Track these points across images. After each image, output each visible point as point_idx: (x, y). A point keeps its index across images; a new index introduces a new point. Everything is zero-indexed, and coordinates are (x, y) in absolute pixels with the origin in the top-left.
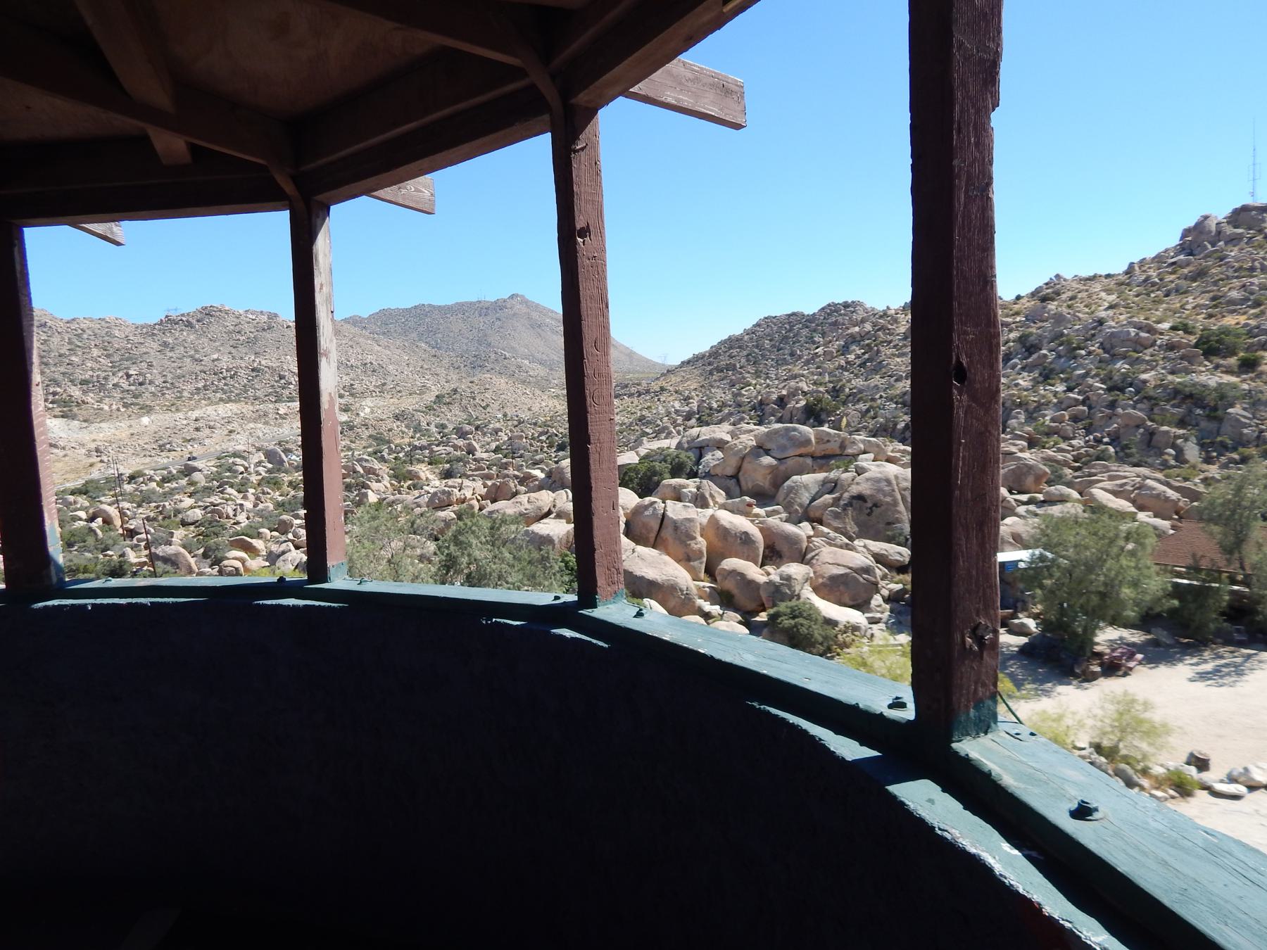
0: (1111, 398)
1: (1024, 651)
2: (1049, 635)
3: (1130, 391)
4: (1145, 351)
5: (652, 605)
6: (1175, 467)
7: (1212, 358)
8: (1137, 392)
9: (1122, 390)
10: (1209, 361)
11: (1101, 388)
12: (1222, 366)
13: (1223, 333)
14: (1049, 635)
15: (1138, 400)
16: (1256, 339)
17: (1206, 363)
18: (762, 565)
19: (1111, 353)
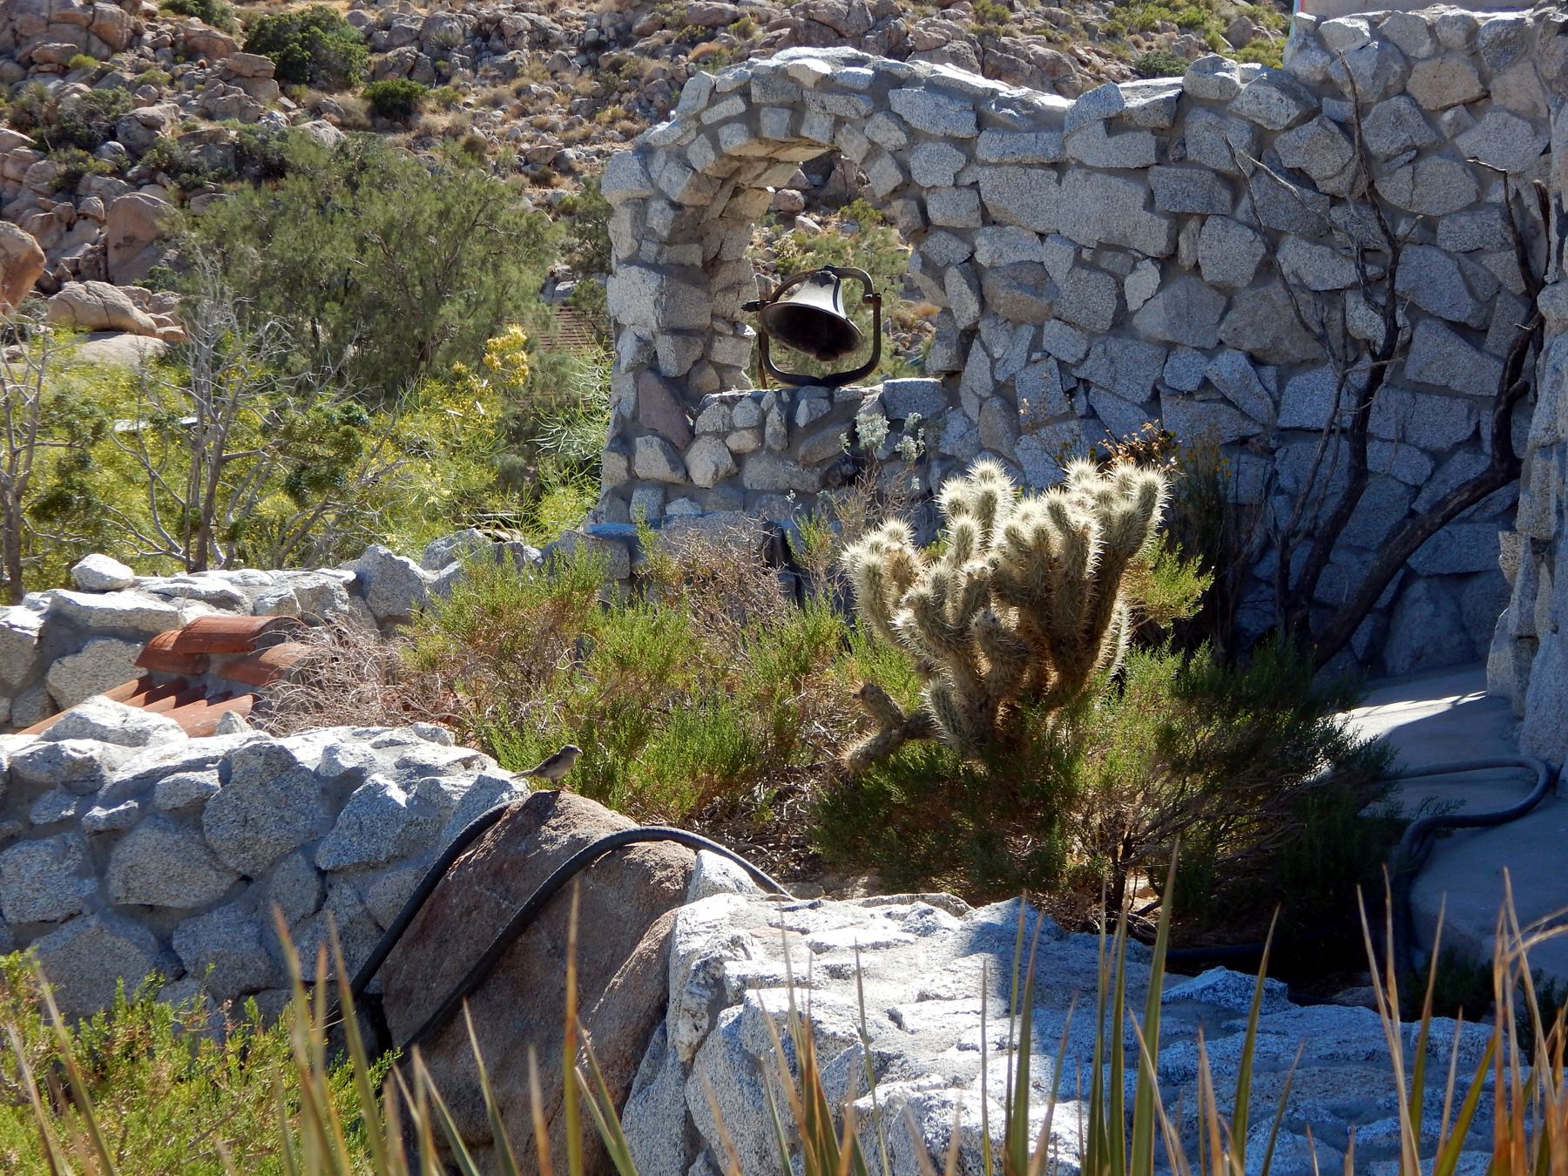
0: (63, 168)
1: (1073, 724)
2: (1026, 677)
3: (115, 150)
4: (118, 57)
5: (1107, 1012)
6: (1252, 198)
7: (296, 89)
8: (135, 153)
9: (90, 145)
10: (292, 98)
11: (24, 142)
12: (328, 108)
13: (316, 22)
14: (1026, 677)
15: (139, 176)
16: (390, 54)
17: (285, 101)
18: (610, 272)
19: (19, 54)
